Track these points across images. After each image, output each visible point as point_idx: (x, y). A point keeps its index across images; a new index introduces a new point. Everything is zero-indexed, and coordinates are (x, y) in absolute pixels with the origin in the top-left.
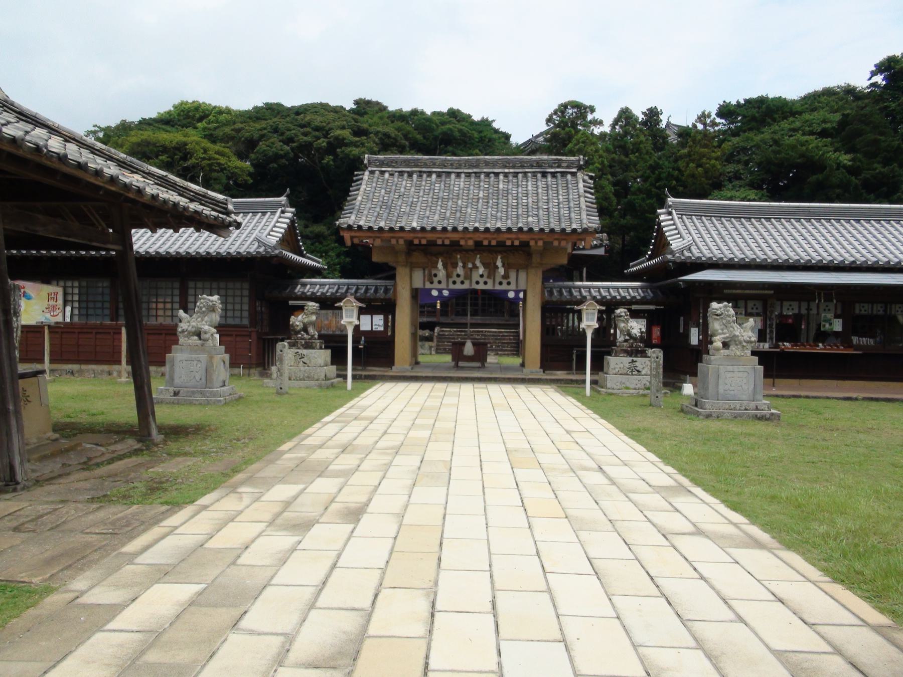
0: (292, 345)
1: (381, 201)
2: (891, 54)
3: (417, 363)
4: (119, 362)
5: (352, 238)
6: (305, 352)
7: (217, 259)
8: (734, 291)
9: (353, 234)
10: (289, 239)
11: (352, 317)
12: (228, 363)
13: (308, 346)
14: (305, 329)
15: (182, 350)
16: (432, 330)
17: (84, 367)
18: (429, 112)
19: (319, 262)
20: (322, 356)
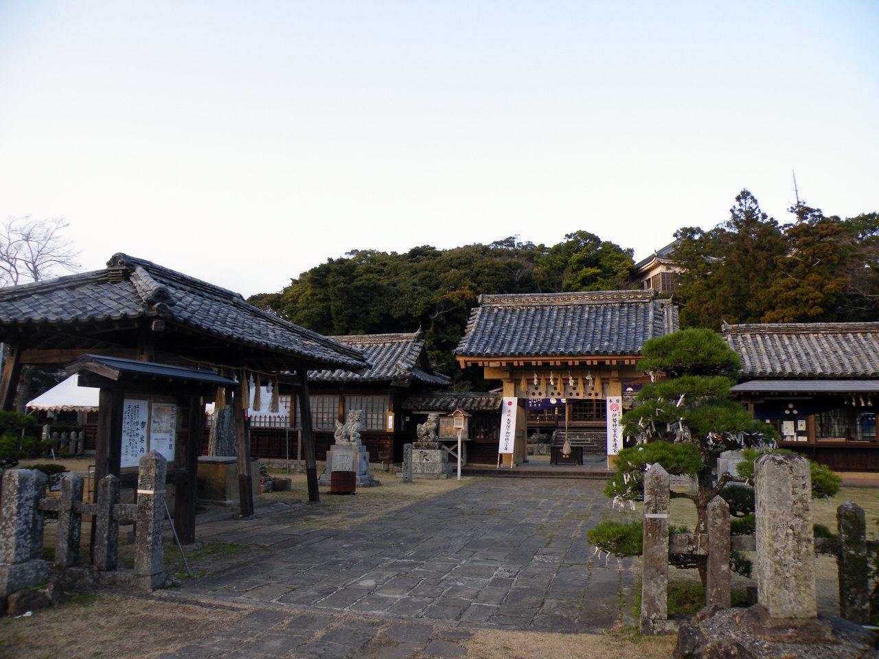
0: (417, 447)
1: (491, 329)
2: (113, 254)
3: (525, 461)
4: (296, 458)
5: (466, 362)
6: (427, 451)
7: (380, 382)
8: (807, 398)
9: (467, 359)
10: (423, 362)
11: (460, 424)
12: (368, 458)
13: (429, 447)
14: (427, 434)
15: (337, 448)
16: (551, 433)
17: (272, 460)
18: (843, 219)
19: (445, 379)
20: (436, 456)
